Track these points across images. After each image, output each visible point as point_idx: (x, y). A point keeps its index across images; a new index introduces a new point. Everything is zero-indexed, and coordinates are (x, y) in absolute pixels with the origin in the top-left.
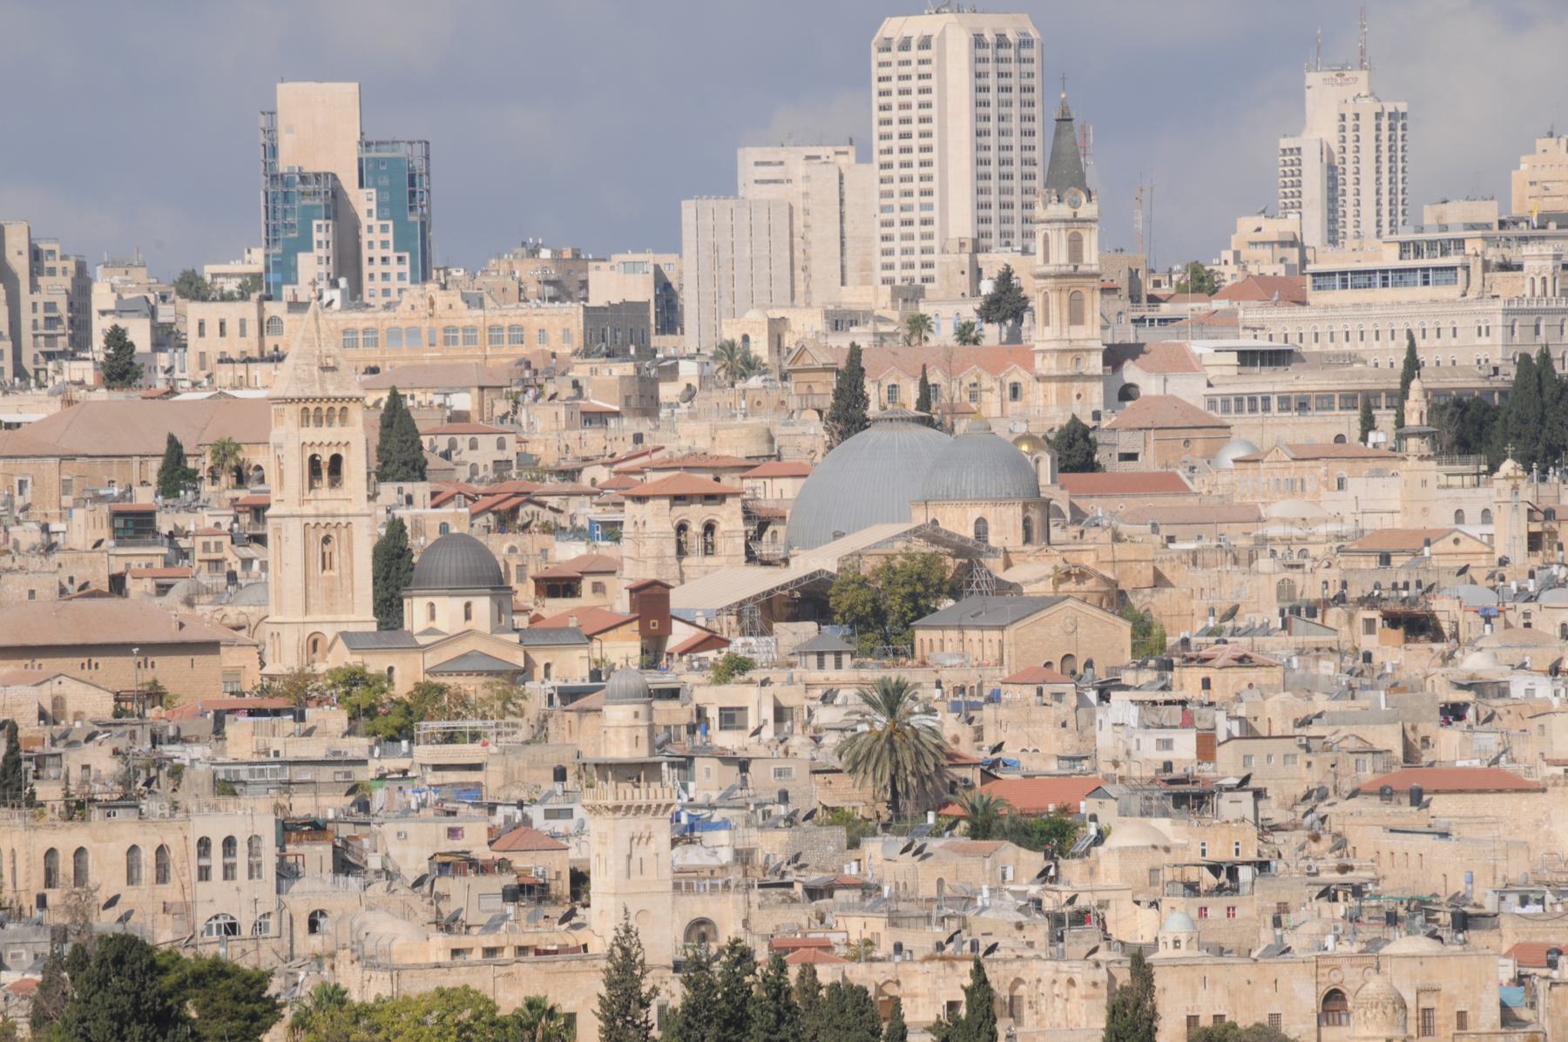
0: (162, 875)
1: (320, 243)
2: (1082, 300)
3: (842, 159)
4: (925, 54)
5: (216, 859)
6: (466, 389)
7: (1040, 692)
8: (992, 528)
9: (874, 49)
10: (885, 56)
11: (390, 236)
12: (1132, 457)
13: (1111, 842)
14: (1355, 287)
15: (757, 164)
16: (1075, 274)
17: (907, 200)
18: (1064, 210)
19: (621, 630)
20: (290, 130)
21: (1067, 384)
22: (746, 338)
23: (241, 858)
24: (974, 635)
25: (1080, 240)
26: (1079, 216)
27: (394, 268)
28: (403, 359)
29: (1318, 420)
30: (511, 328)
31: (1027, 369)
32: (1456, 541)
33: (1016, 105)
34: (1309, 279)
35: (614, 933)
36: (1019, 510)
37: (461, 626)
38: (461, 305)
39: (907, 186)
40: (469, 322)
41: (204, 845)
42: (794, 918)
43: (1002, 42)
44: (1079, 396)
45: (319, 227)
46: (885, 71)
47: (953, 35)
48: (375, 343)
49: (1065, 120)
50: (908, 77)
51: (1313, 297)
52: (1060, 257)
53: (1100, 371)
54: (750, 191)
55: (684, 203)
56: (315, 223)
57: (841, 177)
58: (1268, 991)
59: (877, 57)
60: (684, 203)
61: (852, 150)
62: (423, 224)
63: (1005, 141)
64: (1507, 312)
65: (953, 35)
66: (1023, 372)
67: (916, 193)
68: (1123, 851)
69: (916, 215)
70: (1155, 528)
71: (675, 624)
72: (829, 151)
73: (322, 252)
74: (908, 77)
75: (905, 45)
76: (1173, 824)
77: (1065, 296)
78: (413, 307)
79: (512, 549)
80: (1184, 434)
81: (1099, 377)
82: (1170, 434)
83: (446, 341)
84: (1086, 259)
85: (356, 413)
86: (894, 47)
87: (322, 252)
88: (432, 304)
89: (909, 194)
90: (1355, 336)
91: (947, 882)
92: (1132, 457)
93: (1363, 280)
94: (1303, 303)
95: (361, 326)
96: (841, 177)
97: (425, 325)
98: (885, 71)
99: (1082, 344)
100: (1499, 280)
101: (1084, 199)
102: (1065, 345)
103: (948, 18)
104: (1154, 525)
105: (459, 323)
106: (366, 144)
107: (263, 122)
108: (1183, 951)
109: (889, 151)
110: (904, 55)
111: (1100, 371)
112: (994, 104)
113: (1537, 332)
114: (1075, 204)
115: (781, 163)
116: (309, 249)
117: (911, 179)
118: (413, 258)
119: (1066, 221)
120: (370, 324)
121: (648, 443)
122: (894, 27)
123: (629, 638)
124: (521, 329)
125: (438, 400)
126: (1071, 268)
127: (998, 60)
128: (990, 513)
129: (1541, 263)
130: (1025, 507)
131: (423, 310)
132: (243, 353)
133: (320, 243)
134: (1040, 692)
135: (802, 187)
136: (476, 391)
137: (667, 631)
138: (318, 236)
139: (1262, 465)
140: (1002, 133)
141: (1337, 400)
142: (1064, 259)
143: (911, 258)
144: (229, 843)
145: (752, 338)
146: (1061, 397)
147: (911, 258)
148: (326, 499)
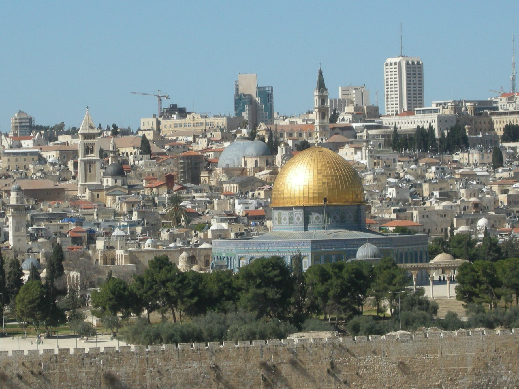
4: (395, 66)
6: (191, 136)
10: (387, 67)
37: (114, 184)
38: (200, 118)
40: (202, 121)
46: (387, 70)
48: (181, 126)
68: (212, 230)
75: (391, 64)
83: (197, 126)
88: (194, 117)
93: (427, 112)
97: (192, 123)
105: (200, 122)
108: (150, 248)
110: (391, 67)
116: (245, 111)
118: (269, 113)
125: (185, 139)
131: (192, 119)
138: (247, 108)
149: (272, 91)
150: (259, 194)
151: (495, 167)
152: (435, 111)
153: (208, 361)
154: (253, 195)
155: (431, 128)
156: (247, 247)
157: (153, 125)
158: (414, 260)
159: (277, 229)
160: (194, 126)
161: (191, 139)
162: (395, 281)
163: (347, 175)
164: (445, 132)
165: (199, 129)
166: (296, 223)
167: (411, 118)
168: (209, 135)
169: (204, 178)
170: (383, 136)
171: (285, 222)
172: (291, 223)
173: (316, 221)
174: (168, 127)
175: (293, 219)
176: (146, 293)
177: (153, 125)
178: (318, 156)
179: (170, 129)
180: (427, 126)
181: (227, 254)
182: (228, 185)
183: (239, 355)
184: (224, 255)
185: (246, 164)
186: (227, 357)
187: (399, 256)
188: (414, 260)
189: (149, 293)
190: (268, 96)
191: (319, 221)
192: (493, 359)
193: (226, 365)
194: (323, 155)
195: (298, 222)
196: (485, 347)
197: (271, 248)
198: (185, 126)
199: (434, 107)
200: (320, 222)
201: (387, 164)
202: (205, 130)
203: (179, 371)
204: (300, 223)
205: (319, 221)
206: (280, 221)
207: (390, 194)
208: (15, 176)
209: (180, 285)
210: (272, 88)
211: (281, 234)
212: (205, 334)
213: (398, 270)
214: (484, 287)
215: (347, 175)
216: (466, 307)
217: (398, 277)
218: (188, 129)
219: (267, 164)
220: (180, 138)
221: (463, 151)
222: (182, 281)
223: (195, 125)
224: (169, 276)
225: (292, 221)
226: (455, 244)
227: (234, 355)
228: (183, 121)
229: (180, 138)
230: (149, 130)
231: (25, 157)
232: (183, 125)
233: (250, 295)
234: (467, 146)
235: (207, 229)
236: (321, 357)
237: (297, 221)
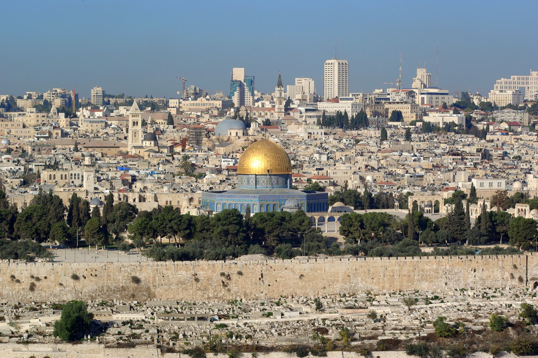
0: (66, 178)
5: (73, 177)
12: (43, 116)
18: (279, 89)
23: (77, 177)
27: (248, 94)
35: (512, 213)
37: (150, 145)
41: (71, 175)
43: (343, 64)
49: (280, 76)
51: (340, 102)
52: (278, 95)
54: (296, 84)
65: (335, 62)
75: (329, 64)
85: (140, 116)
92: (43, 116)
122: (328, 61)
144: (75, 175)
148: (135, 127)
151: (382, 140)
152: (352, 99)
153: (192, 271)
154: (232, 156)
155: (346, 113)
161: (199, 114)
165: (204, 108)
168: (210, 112)
170: (317, 117)
174: (186, 105)
176: (160, 226)
180: (343, 110)
183: (209, 268)
184: (208, 201)
186: (202, 269)
187: (310, 206)
188: (316, 209)
189: (161, 227)
192: (354, 274)
193: (201, 274)
196: (350, 267)
198: (197, 105)
199: (351, 96)
203: (175, 276)
208: (91, 136)
212: (191, 255)
214: (355, 228)
216: (344, 239)
217: (305, 222)
218: (198, 107)
219: (243, 135)
220: (193, 113)
221: (364, 129)
226: (347, 196)
227: (206, 268)
229: (193, 113)
231: (97, 124)
233: (219, 230)
234: (367, 126)
236: (256, 271)
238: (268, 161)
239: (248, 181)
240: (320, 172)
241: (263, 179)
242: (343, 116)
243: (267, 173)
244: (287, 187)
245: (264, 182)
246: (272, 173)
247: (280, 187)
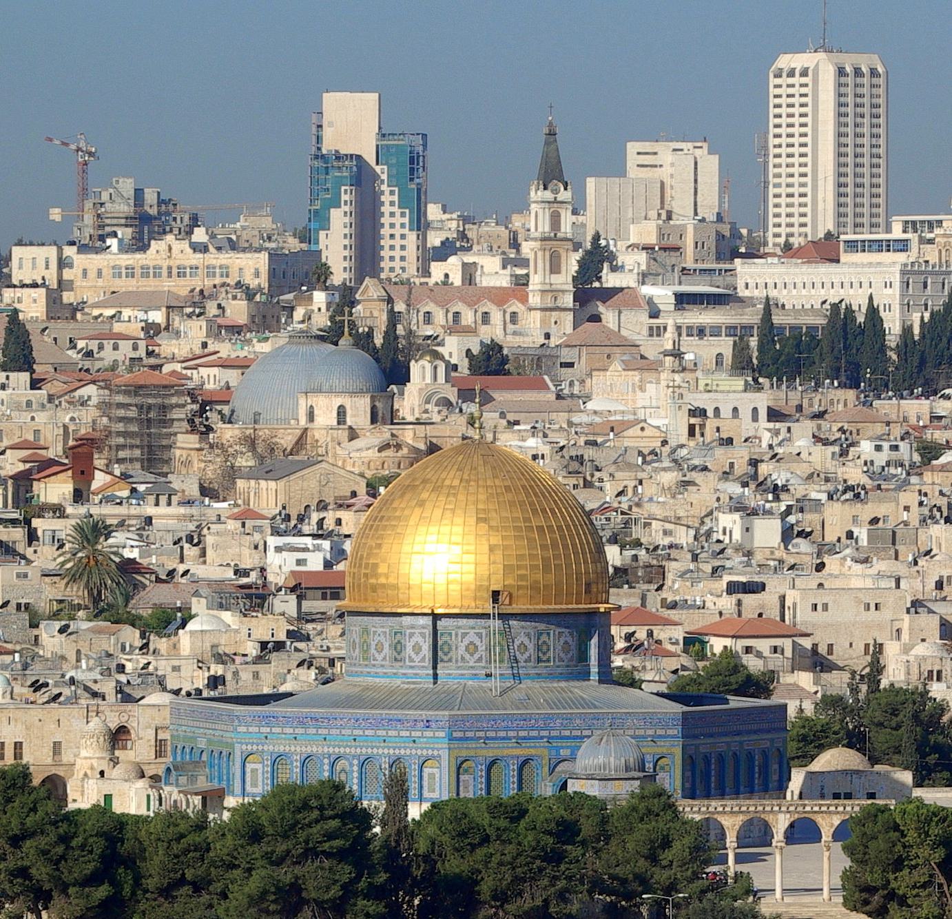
1: (346, 202)
2: (559, 257)
3: (698, 152)
4: (804, 80)
6: (158, 308)
7: (243, 525)
8: (349, 412)
9: (771, 76)
10: (778, 81)
11: (396, 198)
13: (191, 626)
14: (894, 251)
15: (639, 153)
16: (555, 238)
17: (790, 180)
18: (548, 195)
19: (60, 476)
20: (331, 124)
21: (548, 313)
22: (447, 276)
24: (263, 483)
25: (559, 215)
26: (558, 199)
27: (398, 220)
28: (150, 286)
29: (706, 343)
30: (221, 267)
31: (523, 303)
32: (642, 429)
33: (867, 116)
34: (842, 243)
36: (368, 400)
38: (190, 251)
39: (790, 170)
40: (194, 263)
42: (388, 680)
43: (858, 72)
44: (556, 323)
45: (346, 191)
46: (778, 91)
47: (824, 66)
50: (793, 96)
51: (844, 257)
52: (545, 227)
53: (571, 305)
54: (633, 171)
55: (588, 179)
56: (343, 188)
57: (696, 163)
58: (53, 726)
59: (773, 81)
60: (588, 179)
61: (705, 145)
62: (419, 190)
63: (859, 141)
64: (903, 273)
65: (824, 66)
66: (520, 305)
67: (797, 175)
68: (192, 633)
69: (796, 190)
70: (503, 415)
71: (96, 471)
72: (690, 145)
73: (347, 208)
74: (793, 96)
75: (791, 74)
76: (232, 615)
77: (547, 254)
78: (157, 252)
79: (72, 419)
80: (607, 350)
81: (570, 310)
82: (598, 350)
84: (563, 230)
86: (784, 75)
87: (347, 208)
88: (170, 249)
89: (792, 175)
90: (847, 285)
91: (83, 652)
93: (875, 247)
94: (838, 261)
95: (124, 264)
96: (696, 163)
97: (165, 264)
98: (778, 91)
99: (559, 287)
100: (929, 250)
101: (562, 189)
102: (547, 287)
103: (821, 56)
104: (502, 413)
105: (187, 263)
106: (382, 135)
107: (314, 118)
109: (780, 146)
110: (790, 81)
111: (571, 305)
112: (851, 115)
113: (925, 286)
114: (556, 192)
115: (655, 153)
117: (793, 165)
119: (549, 202)
120: (130, 262)
121: (211, 348)
122: (785, 61)
123: (65, 482)
124: (227, 267)
125: (141, 315)
126: (552, 235)
127: (872, 86)
128: (347, 402)
129: (945, 240)
130: (373, 398)
131: (164, 254)
132: (21, 281)
133: (346, 202)
134: (243, 525)
135: (671, 170)
136: (164, 309)
137: (91, 478)
138: (344, 197)
139: (608, 373)
140: (856, 135)
141: (724, 330)
142: (547, 229)
143: (792, 220)
145: (451, 276)
146: (543, 321)
147: (792, 220)
149: (425, 146)
150: (339, 522)
152: (903, 246)
154: (321, 523)
155: (873, 312)
156: (268, 725)
157: (47, 267)
158: (729, 782)
159: (357, 674)
160: (170, 275)
161: (157, 317)
162: (666, 856)
163: (568, 526)
164: (916, 317)
165: (181, 287)
166: (411, 660)
167: (824, 271)
168: (212, 309)
169: (185, 453)
171: (379, 657)
172: (396, 659)
173: (467, 656)
174: (92, 274)
175: (403, 647)
177: (47, 267)
178: (481, 469)
179: (100, 282)
181: (210, 742)
182: (253, 482)
184: (202, 743)
185: (311, 416)
187: (700, 765)
188: (729, 782)
190: (412, 161)
191: (476, 656)
194: (494, 468)
195: (417, 659)
197: (334, 731)
198: (145, 275)
199: (897, 233)
200: (480, 659)
201: (725, 436)
202: (202, 292)
204: (423, 660)
205: (476, 656)
206: (366, 652)
207: (724, 533)
209: (60, 849)
210: (424, 136)
211: (367, 688)
213: (678, 825)
215: (568, 526)
217: (677, 845)
218: (150, 284)
219: (374, 420)
220: (126, 313)
222: (65, 839)
223: (175, 271)
224: (29, 821)
225: (399, 653)
226: (879, 716)
228: (137, 259)
229: (126, 313)
230: (35, 285)
232: (138, 271)
233: (254, 884)
235: (178, 628)
237: (414, 656)
238: (492, 549)
239: (398, 647)
240: (749, 600)
241: (472, 637)
242: (862, 330)
243: (488, 608)
244: (585, 676)
245: (472, 648)
246: (517, 608)
247: (551, 677)
